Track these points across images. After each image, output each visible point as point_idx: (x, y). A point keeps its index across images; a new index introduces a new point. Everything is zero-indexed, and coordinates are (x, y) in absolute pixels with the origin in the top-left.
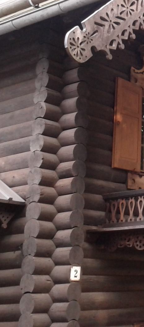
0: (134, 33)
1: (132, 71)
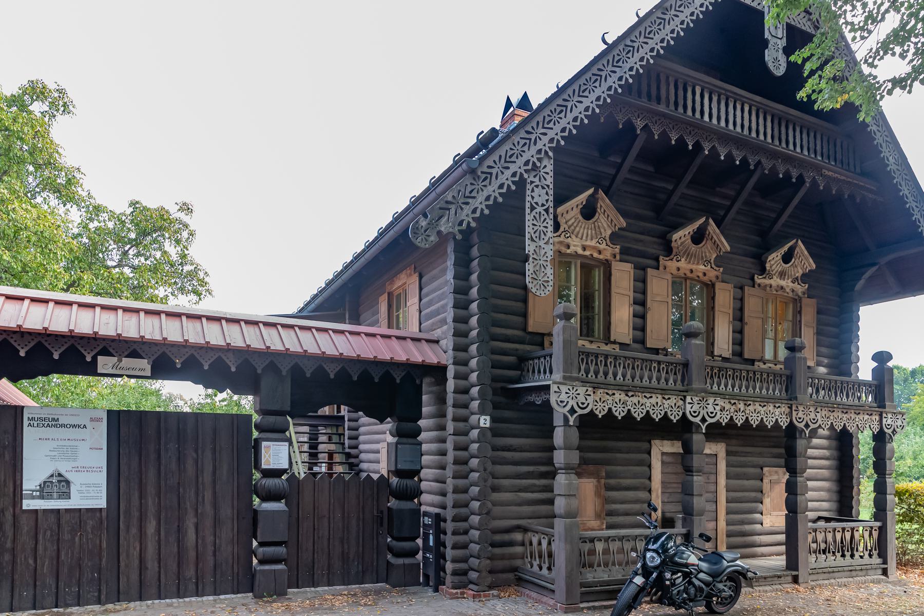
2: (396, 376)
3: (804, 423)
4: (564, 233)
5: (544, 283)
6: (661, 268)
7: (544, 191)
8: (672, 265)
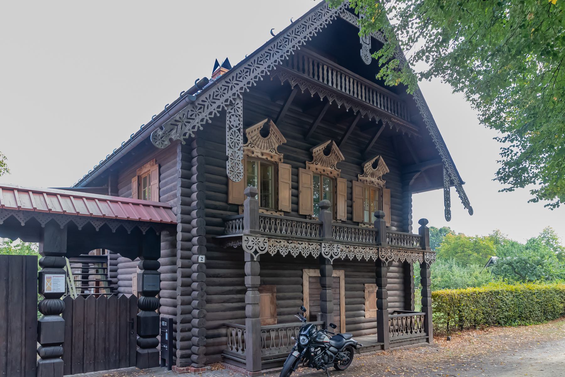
0: (201, 126)
1: (359, 176)
3: (329, 255)
6: (307, 168)
7: (237, 118)
8: (313, 167)
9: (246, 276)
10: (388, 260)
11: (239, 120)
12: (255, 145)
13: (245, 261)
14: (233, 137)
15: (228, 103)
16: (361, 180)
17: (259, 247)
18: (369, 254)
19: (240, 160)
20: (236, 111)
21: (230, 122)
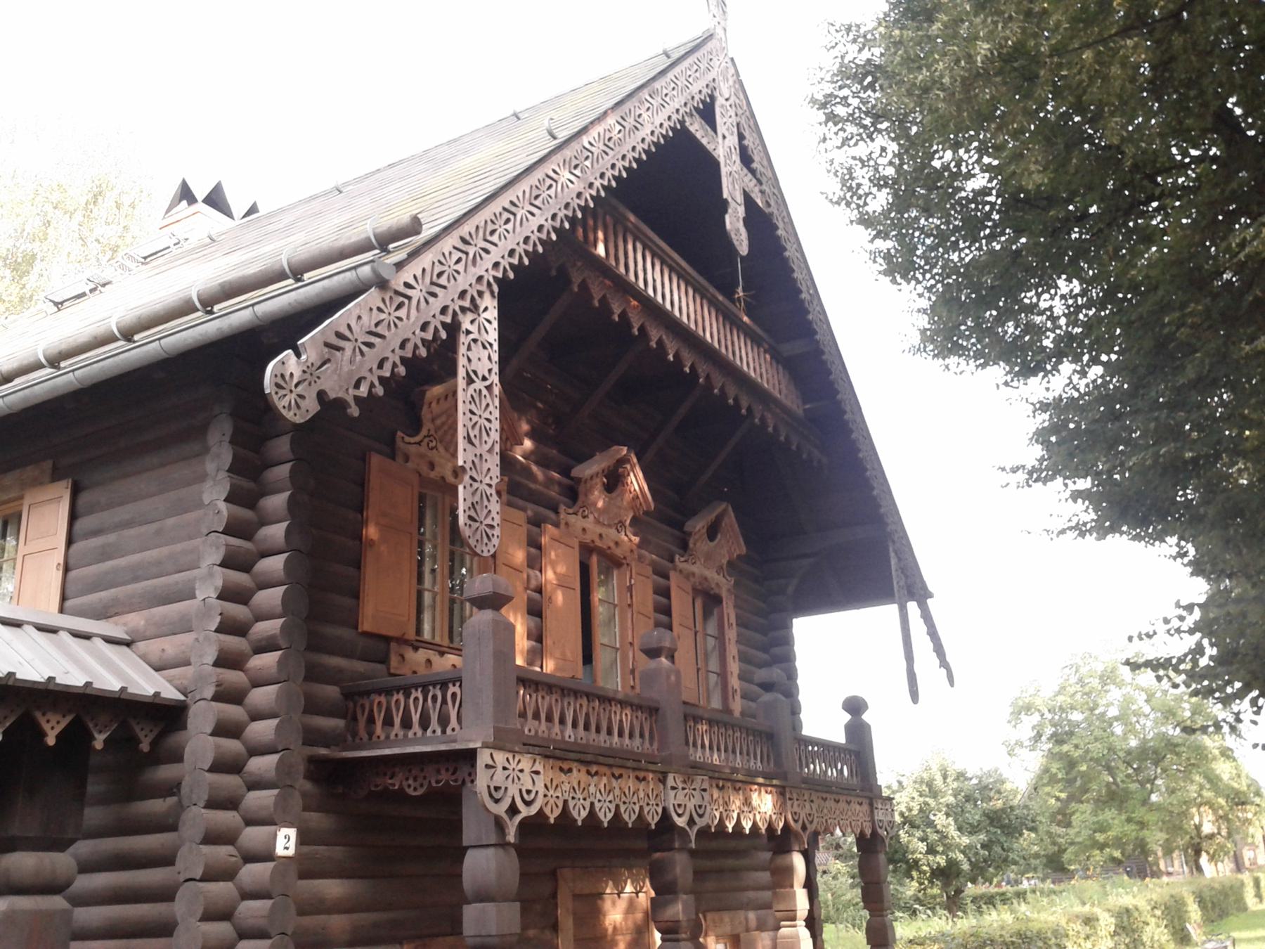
2: (47, 727)
3: (506, 804)
4: (426, 440)
5: (487, 530)
6: (562, 526)
7: (486, 353)
8: (577, 522)
9: (469, 903)
10: (695, 823)
11: (489, 358)
12: (441, 442)
13: (465, 843)
14: (475, 411)
15: (467, 304)
16: (681, 571)
17: (520, 790)
18: (611, 797)
19: (494, 482)
20: (483, 330)
21: (469, 360)
